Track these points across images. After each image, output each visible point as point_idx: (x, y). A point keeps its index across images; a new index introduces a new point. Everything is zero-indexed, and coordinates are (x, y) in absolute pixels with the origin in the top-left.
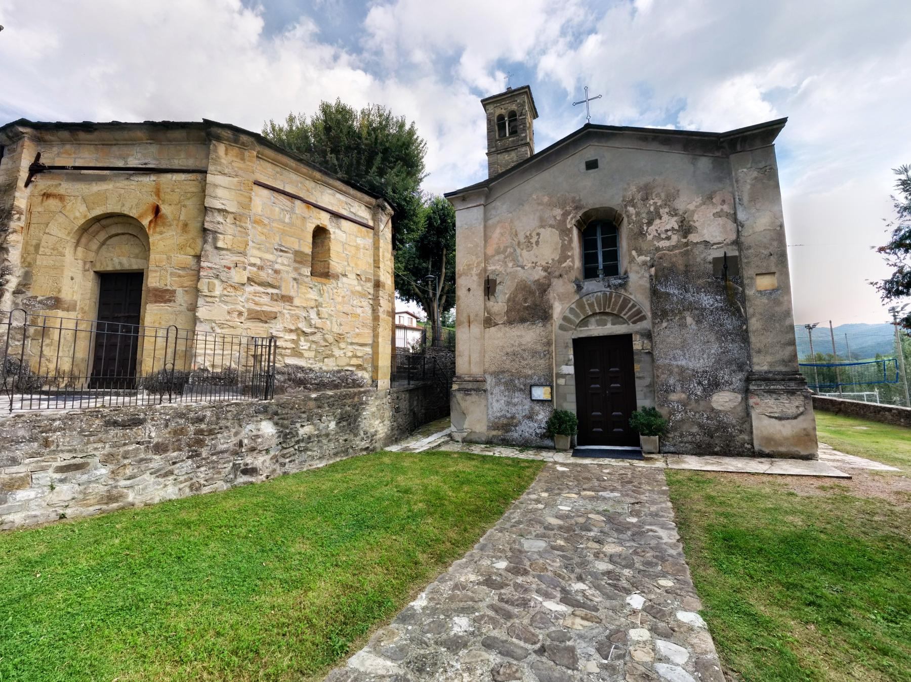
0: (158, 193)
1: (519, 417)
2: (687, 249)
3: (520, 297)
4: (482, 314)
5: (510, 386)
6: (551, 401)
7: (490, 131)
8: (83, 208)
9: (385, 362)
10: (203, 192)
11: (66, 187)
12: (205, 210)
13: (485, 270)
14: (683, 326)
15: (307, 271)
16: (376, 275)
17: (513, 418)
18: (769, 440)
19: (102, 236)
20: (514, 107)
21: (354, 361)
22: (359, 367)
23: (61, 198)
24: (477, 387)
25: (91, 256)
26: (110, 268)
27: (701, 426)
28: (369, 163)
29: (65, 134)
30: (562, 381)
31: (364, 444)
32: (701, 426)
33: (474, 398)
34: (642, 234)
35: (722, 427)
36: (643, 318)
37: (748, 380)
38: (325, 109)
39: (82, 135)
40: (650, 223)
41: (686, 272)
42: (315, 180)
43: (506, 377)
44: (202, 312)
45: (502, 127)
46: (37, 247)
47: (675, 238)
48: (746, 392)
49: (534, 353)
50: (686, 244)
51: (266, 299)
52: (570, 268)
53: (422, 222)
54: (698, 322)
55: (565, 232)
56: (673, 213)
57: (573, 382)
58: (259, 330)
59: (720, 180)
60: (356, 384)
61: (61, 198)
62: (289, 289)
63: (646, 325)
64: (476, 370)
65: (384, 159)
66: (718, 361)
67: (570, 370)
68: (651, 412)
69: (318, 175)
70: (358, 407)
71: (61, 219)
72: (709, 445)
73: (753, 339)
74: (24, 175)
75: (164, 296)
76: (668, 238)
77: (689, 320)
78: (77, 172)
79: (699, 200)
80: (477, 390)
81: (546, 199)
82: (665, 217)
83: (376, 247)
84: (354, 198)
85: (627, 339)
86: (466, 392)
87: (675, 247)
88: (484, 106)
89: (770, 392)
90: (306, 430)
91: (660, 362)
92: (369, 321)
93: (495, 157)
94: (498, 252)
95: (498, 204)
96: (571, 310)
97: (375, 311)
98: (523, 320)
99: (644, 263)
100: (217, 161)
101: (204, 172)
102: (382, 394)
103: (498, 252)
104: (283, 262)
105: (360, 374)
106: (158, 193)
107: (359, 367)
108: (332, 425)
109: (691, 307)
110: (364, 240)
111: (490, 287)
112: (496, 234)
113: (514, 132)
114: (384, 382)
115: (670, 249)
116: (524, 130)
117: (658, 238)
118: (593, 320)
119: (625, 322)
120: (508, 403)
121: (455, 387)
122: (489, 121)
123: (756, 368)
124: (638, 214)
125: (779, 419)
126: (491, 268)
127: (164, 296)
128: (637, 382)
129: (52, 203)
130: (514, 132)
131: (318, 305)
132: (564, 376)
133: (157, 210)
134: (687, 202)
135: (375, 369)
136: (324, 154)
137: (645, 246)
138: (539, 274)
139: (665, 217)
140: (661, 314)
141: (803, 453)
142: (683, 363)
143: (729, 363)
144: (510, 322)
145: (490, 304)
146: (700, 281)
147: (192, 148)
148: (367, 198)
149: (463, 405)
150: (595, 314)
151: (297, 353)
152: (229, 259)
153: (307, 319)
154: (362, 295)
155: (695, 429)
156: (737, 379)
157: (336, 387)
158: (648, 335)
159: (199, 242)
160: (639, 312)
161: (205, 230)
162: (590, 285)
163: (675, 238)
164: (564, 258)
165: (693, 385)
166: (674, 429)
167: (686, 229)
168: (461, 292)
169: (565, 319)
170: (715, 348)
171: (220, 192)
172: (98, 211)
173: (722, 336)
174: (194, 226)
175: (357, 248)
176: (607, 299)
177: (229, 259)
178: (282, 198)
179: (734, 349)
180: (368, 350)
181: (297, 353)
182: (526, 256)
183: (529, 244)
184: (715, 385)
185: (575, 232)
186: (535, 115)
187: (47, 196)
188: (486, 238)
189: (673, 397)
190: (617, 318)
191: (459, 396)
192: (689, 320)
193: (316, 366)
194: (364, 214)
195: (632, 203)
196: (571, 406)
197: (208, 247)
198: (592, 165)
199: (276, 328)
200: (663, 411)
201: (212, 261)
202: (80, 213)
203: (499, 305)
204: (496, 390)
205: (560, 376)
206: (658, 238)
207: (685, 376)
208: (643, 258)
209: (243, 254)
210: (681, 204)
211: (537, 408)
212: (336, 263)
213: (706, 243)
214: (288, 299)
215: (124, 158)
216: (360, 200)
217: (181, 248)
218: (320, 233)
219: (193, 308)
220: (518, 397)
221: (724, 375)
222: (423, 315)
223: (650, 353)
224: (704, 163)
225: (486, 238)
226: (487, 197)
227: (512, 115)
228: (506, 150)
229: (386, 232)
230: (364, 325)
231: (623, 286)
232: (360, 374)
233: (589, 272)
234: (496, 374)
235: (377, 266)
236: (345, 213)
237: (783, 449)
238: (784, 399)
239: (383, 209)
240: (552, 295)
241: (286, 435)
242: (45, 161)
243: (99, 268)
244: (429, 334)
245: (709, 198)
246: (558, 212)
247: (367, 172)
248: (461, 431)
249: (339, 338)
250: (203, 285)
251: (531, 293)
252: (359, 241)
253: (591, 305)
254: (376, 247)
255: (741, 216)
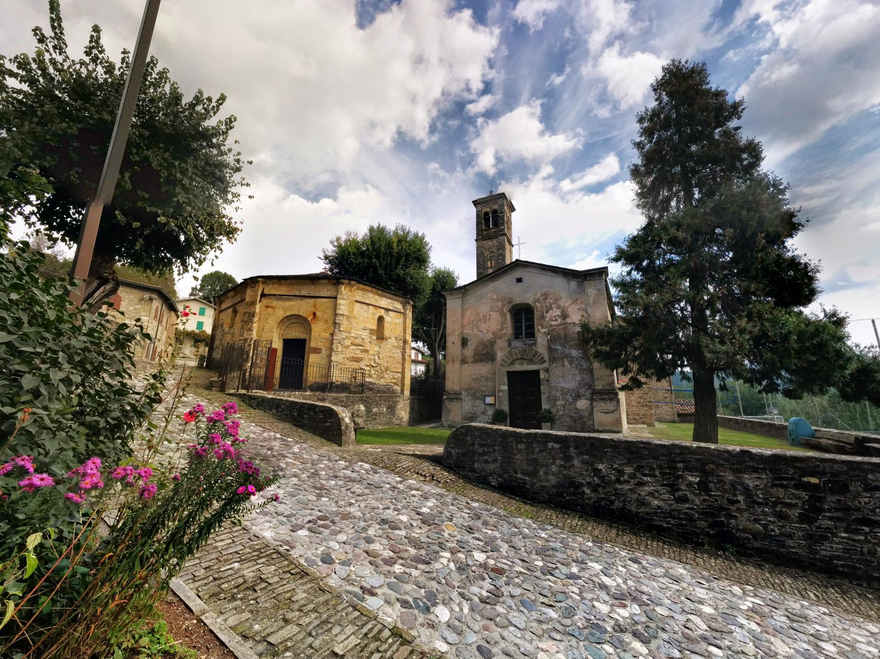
0: (315, 306)
1: (478, 413)
2: (565, 326)
3: (480, 348)
4: (460, 357)
5: (474, 396)
6: (494, 404)
7: (478, 223)
8: (282, 312)
9: (408, 382)
10: (335, 307)
11: (275, 303)
12: (336, 315)
13: (462, 332)
14: (563, 366)
15: (374, 337)
16: (404, 337)
17: (475, 413)
18: (601, 424)
19: (287, 323)
20: (496, 207)
21: (393, 381)
22: (396, 384)
23: (273, 308)
24: (456, 397)
25: (282, 332)
26: (291, 337)
27: (571, 417)
28: (397, 264)
29: (276, 281)
30: (501, 394)
31: (397, 422)
32: (571, 417)
33: (455, 403)
34: (543, 317)
35: (581, 417)
36: (545, 362)
37: (593, 394)
38: (371, 229)
39: (283, 281)
40: (547, 312)
41: (565, 338)
42: (379, 295)
43: (472, 391)
44: (334, 358)
45: (487, 220)
46: (263, 329)
47: (559, 320)
48: (592, 400)
49: (487, 379)
50: (565, 324)
51: (358, 352)
52: (505, 334)
53: (428, 290)
54: (571, 364)
55: (503, 315)
56: (558, 307)
57: (507, 394)
58: (355, 365)
59: (580, 293)
60: (393, 392)
61: (273, 308)
62: (368, 346)
63: (546, 365)
64: (456, 388)
65: (407, 260)
66: (579, 384)
67: (505, 388)
68: (549, 412)
69: (380, 292)
70: (396, 403)
71: (273, 317)
72: (575, 427)
73: (595, 373)
74: (259, 298)
75: (317, 351)
76: (556, 320)
77: (566, 363)
78: (280, 297)
79: (570, 302)
80: (457, 399)
81: (495, 297)
82: (555, 309)
83: (405, 323)
84: (395, 300)
85: (537, 372)
86: (451, 400)
87: (560, 325)
88: (475, 205)
89: (602, 399)
90: (375, 410)
91: (552, 385)
92: (400, 361)
93: (481, 243)
94: (469, 324)
95: (469, 297)
96: (506, 356)
97: (403, 355)
98: (481, 361)
99: (545, 333)
100: (341, 294)
101: (336, 298)
102: (406, 398)
103: (469, 324)
104: (365, 335)
105: (395, 387)
106: (315, 306)
107: (396, 384)
108: (385, 409)
109: (567, 356)
110: (399, 320)
111: (464, 342)
112: (468, 313)
113: (496, 225)
114: (407, 392)
115: (557, 326)
116: (503, 224)
117: (551, 320)
118: (517, 362)
119: (536, 364)
120: (473, 406)
121: (445, 397)
122: (478, 216)
123: (597, 387)
124: (541, 307)
125: (605, 413)
126: (465, 331)
127: (317, 351)
128: (543, 396)
129: (270, 310)
130: (496, 225)
131: (379, 353)
132: (502, 391)
133: (314, 314)
134: (565, 302)
135: (403, 385)
136: (370, 258)
137: (544, 324)
138: (490, 336)
139: (555, 309)
140: (553, 360)
141: (616, 430)
142: (563, 385)
143: (585, 385)
144: (475, 362)
145: (465, 351)
146: (572, 343)
147: (330, 287)
148: (401, 299)
149: (449, 407)
150: (518, 359)
151: (370, 376)
152: (344, 335)
153: (374, 360)
154: (398, 347)
155: (568, 419)
156: (588, 393)
157: (385, 392)
158: (547, 371)
159: (332, 328)
160: (543, 358)
161: (335, 323)
162: (517, 344)
163: (559, 320)
164: (502, 328)
165: (568, 397)
166: (558, 419)
167: (564, 316)
168: (449, 344)
169: (503, 360)
170: (578, 378)
171: (342, 307)
172: (289, 314)
173: (581, 371)
174: (331, 321)
175: (396, 324)
176: (524, 351)
177: (344, 335)
178: (364, 306)
179: (587, 377)
180: (400, 375)
181: (370, 376)
182: (484, 326)
183: (485, 320)
184: (578, 397)
185: (508, 315)
186: (512, 209)
187: (267, 307)
188: (463, 315)
189: (559, 403)
190: (531, 361)
191: (447, 402)
192: (566, 363)
193: (377, 382)
194: (399, 306)
195: (538, 301)
196: (506, 407)
197: (336, 330)
198: (519, 280)
199: (362, 365)
200: (554, 411)
201: (338, 336)
202: (280, 314)
203: (469, 352)
204: (467, 399)
205: (500, 391)
206: (551, 320)
207: (564, 392)
208: (544, 330)
209: (350, 333)
210: (562, 303)
211: (488, 408)
212: (387, 333)
213: (574, 323)
214: (367, 351)
215: (299, 290)
216: (398, 301)
217: (325, 331)
218: (381, 319)
219: (330, 356)
220: (478, 402)
221: (582, 391)
222: (425, 350)
223: (548, 380)
224: (573, 284)
225: (463, 315)
226: (464, 294)
227: (495, 212)
228: (490, 238)
229: (410, 314)
230: (398, 362)
231: (535, 344)
232: (395, 387)
233: (517, 335)
234: (467, 390)
235: (405, 332)
236: (391, 308)
237: (607, 428)
238: (608, 402)
239: (409, 303)
240: (496, 347)
241: (369, 411)
242: (266, 292)
243: (285, 337)
244: (432, 367)
245: (575, 301)
246: (500, 304)
247: (396, 269)
248: (447, 421)
249: (387, 369)
250: (334, 347)
251: (486, 346)
252: (397, 320)
253: (516, 354)
254: (405, 323)
255: (589, 311)
